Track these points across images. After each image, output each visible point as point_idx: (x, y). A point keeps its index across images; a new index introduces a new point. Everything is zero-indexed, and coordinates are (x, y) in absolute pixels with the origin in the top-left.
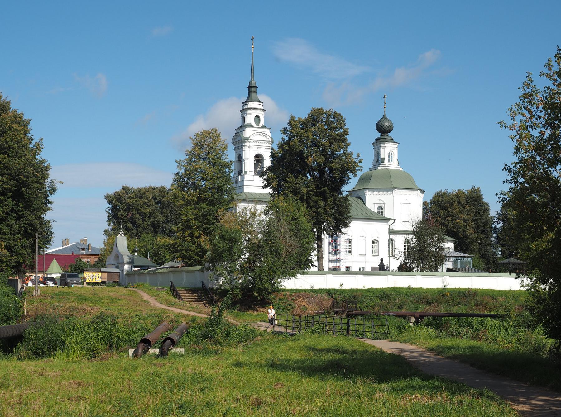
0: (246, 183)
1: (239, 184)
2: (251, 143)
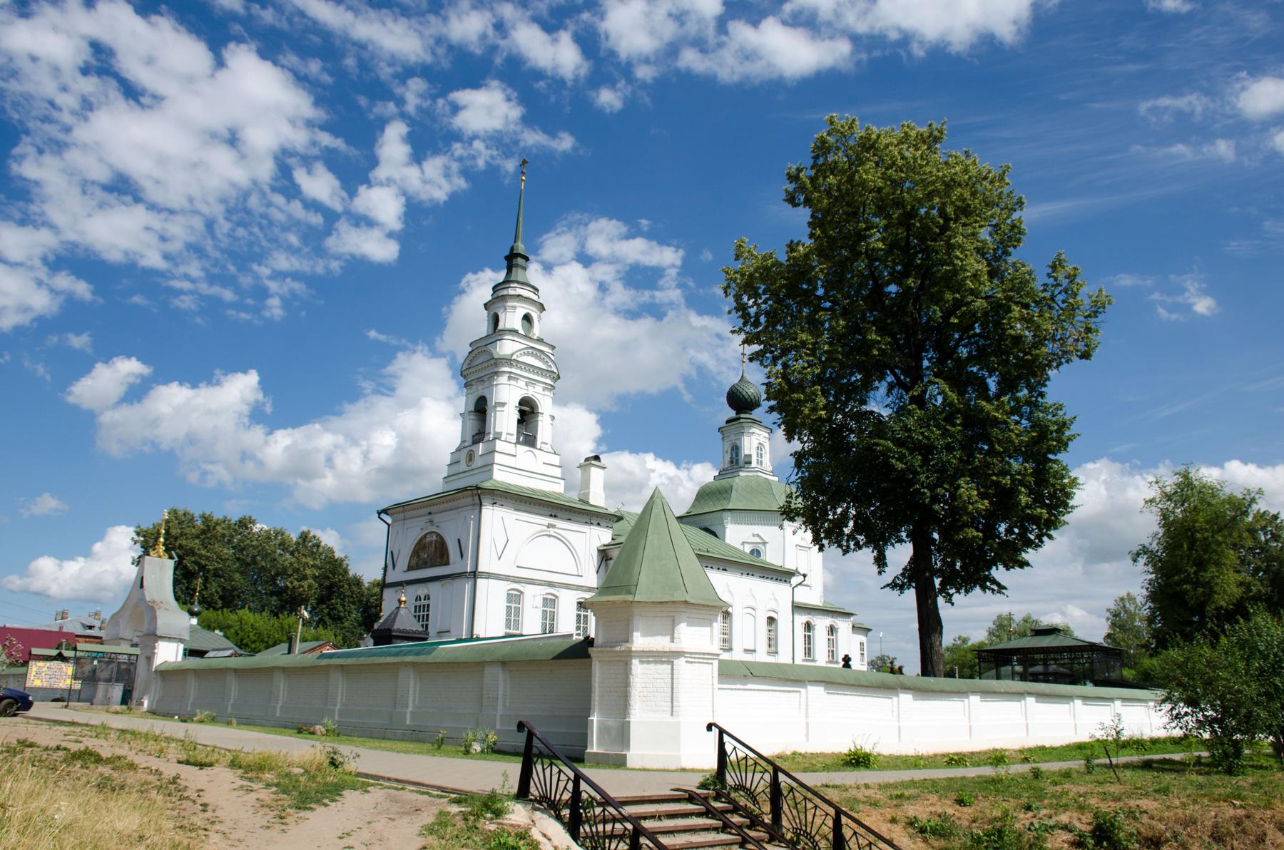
0: (498, 458)
1: (478, 462)
2: (513, 370)
